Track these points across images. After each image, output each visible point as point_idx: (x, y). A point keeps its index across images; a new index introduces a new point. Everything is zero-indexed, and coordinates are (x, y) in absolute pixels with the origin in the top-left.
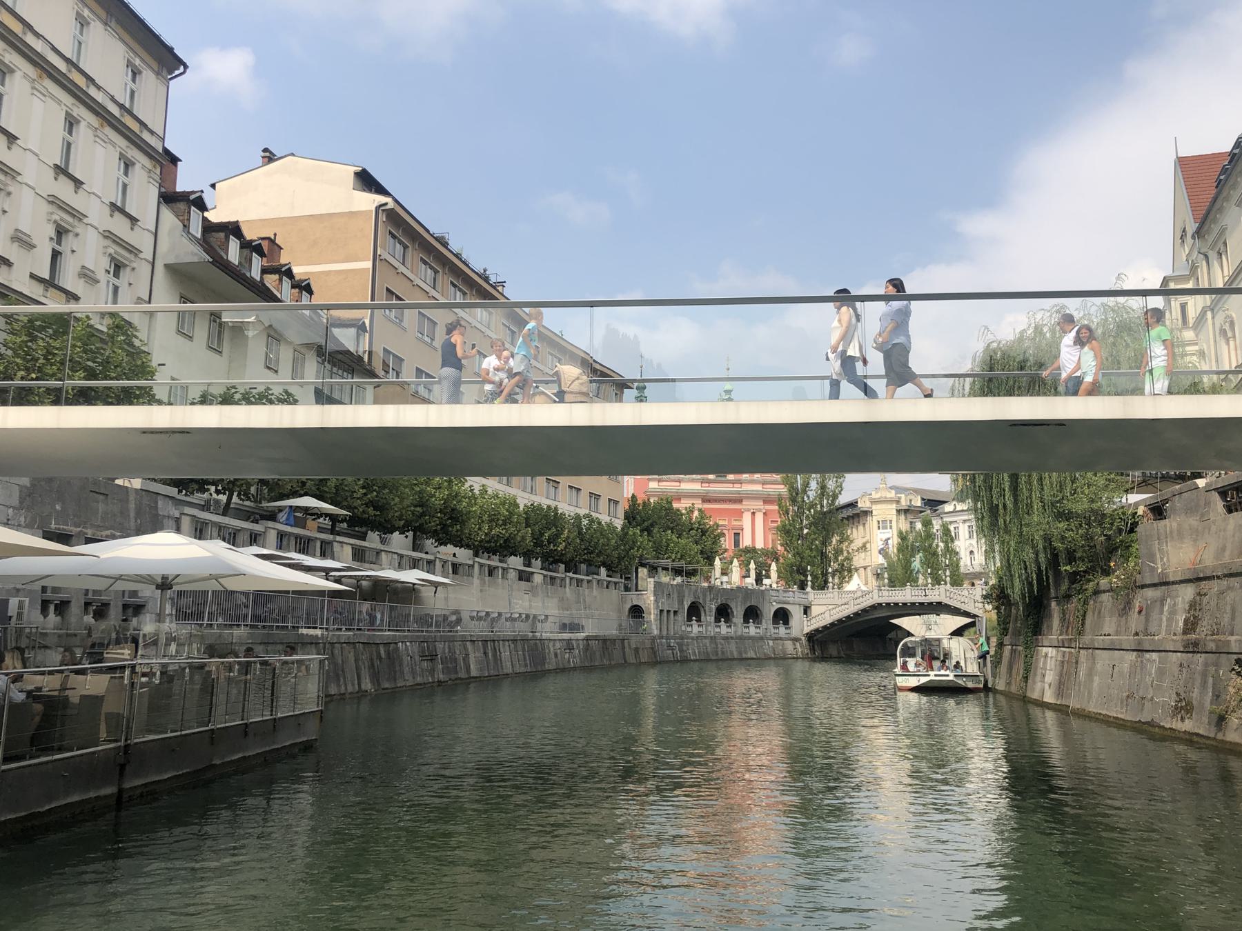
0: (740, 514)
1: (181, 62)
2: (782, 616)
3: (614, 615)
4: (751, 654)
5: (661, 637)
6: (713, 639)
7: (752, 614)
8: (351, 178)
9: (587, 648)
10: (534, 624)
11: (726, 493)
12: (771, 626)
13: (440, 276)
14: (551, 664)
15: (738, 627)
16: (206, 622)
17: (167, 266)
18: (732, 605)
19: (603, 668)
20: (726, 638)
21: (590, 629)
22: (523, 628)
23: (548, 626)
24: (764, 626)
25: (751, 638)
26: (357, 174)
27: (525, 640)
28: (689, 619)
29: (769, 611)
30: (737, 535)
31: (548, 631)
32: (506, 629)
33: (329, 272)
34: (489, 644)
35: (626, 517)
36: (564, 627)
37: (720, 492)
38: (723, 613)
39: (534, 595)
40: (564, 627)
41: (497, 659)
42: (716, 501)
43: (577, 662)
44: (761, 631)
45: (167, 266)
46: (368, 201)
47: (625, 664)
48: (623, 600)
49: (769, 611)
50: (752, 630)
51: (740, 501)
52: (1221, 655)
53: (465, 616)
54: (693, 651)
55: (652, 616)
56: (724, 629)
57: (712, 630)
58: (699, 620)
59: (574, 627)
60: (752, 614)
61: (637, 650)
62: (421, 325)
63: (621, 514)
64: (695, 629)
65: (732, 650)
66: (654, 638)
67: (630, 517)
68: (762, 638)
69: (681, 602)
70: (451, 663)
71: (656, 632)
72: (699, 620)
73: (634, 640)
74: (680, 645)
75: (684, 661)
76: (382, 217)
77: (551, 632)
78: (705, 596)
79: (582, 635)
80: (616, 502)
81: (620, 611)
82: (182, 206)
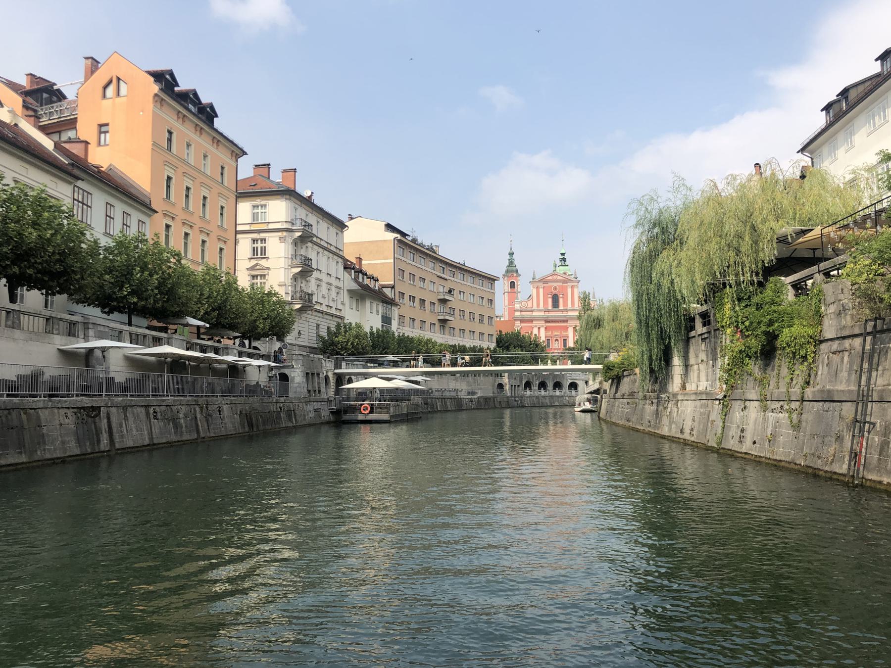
0: (566, 328)
1: (346, 226)
2: (573, 386)
3: (491, 388)
4: (557, 404)
5: (512, 397)
6: (537, 397)
7: (558, 385)
8: (384, 227)
9: (478, 401)
10: (457, 393)
11: (558, 317)
12: (567, 391)
13: (415, 256)
14: (464, 407)
15: (550, 391)
16: (104, 393)
17: (348, 290)
18: (547, 382)
19: (485, 409)
20: (544, 397)
21: (480, 394)
22: (453, 394)
23: (463, 392)
24: (564, 391)
25: (558, 397)
26: (386, 225)
27: (455, 398)
28: (525, 388)
29: (566, 383)
30: (565, 340)
31: (463, 395)
32: (447, 394)
33: (377, 264)
34: (443, 399)
35: (497, 342)
36: (469, 393)
37: (555, 316)
38: (543, 385)
39: (457, 381)
40: (469, 393)
41: (446, 405)
42: (553, 321)
43: (475, 406)
44: (562, 393)
45: (348, 290)
46: (392, 236)
47: (495, 407)
48: (495, 381)
49: (566, 383)
50: (558, 393)
51: (566, 321)
52: (843, 403)
53: (434, 390)
54: (527, 402)
55: (507, 388)
56: (543, 392)
57: (537, 393)
58: (530, 389)
59: (473, 393)
60: (558, 385)
61: (500, 402)
62: (410, 277)
63: (495, 340)
64: (528, 393)
65: (547, 401)
66: (508, 397)
67: (499, 342)
68: (562, 396)
69: (521, 381)
70: (432, 406)
71: (509, 395)
72: (530, 389)
73: (499, 398)
74: (521, 400)
75: (523, 406)
76: (396, 242)
77: (865, 457)
78: (533, 378)
79: (476, 396)
80: (492, 335)
81: (493, 386)
82: (349, 270)
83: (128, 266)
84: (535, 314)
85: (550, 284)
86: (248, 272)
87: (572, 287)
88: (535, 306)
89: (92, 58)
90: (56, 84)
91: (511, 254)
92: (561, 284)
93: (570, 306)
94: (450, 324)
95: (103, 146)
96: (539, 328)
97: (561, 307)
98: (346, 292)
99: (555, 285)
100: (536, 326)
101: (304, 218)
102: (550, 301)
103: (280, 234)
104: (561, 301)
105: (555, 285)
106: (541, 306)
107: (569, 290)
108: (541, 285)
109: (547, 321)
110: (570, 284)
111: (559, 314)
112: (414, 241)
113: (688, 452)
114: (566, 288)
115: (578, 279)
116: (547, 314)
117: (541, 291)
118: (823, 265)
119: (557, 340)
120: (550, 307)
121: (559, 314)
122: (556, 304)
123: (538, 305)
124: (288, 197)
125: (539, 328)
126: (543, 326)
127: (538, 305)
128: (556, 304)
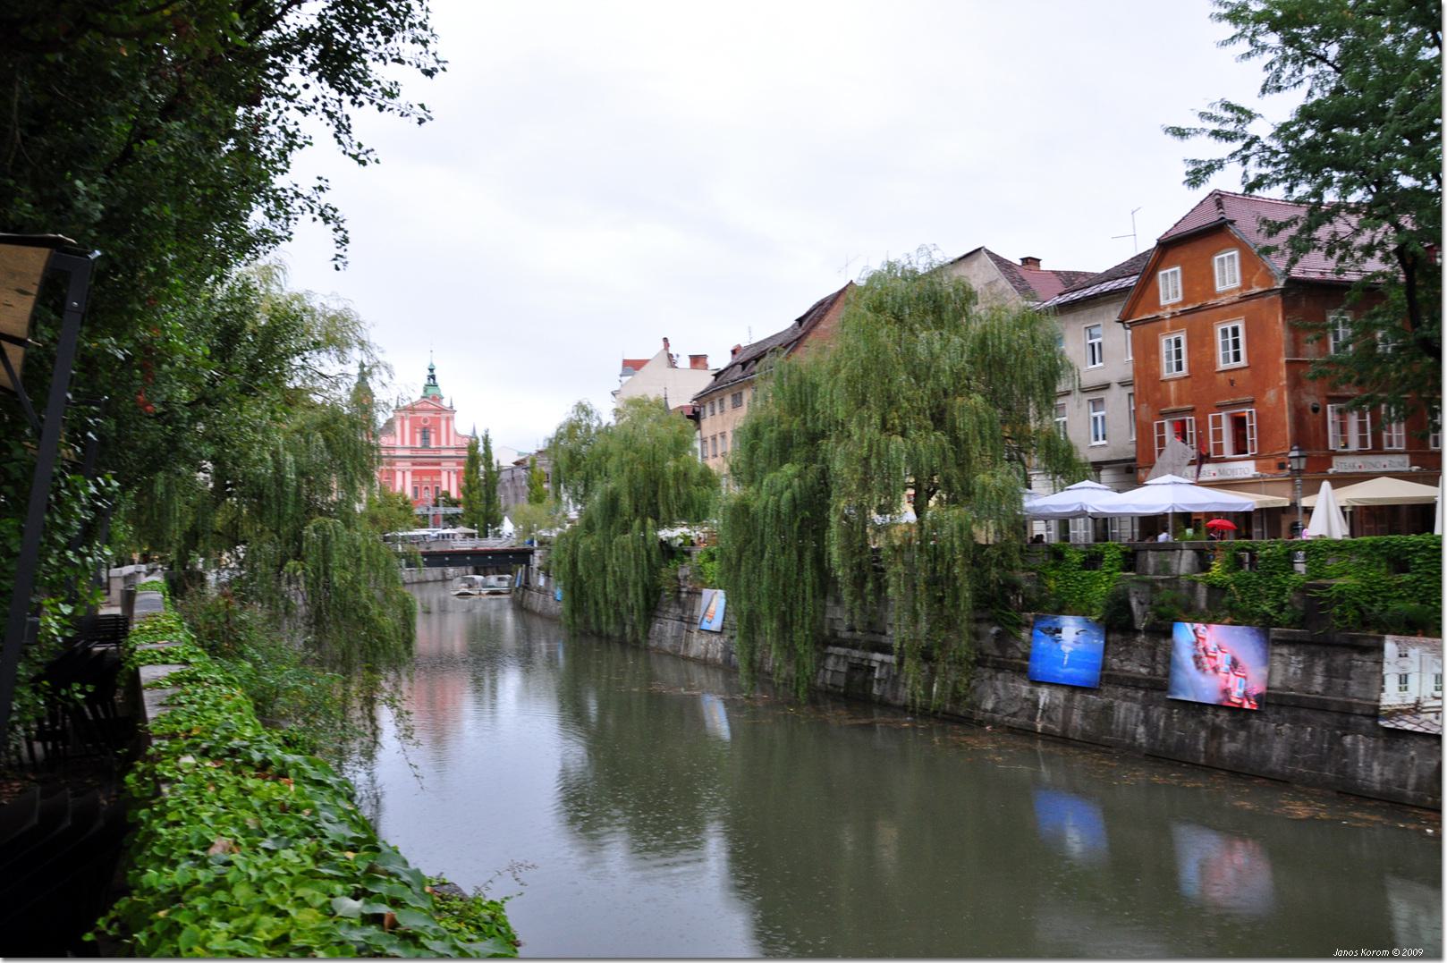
0: (439, 473)
84: (444, 453)
85: (418, 415)
86: (480, 434)
87: (448, 419)
88: (399, 444)
92: (432, 415)
93: (444, 444)
95: (1442, 730)
96: (404, 473)
97: (433, 446)
102: (418, 436)
104: (433, 437)
106: (407, 444)
107: (443, 423)
110: (444, 415)
113: (539, 609)
114: (438, 420)
116: (414, 454)
117: (407, 423)
118: (303, 869)
119: (427, 488)
122: (426, 438)
123: (448, 443)
125: (404, 473)
127: (448, 443)
128: (426, 438)
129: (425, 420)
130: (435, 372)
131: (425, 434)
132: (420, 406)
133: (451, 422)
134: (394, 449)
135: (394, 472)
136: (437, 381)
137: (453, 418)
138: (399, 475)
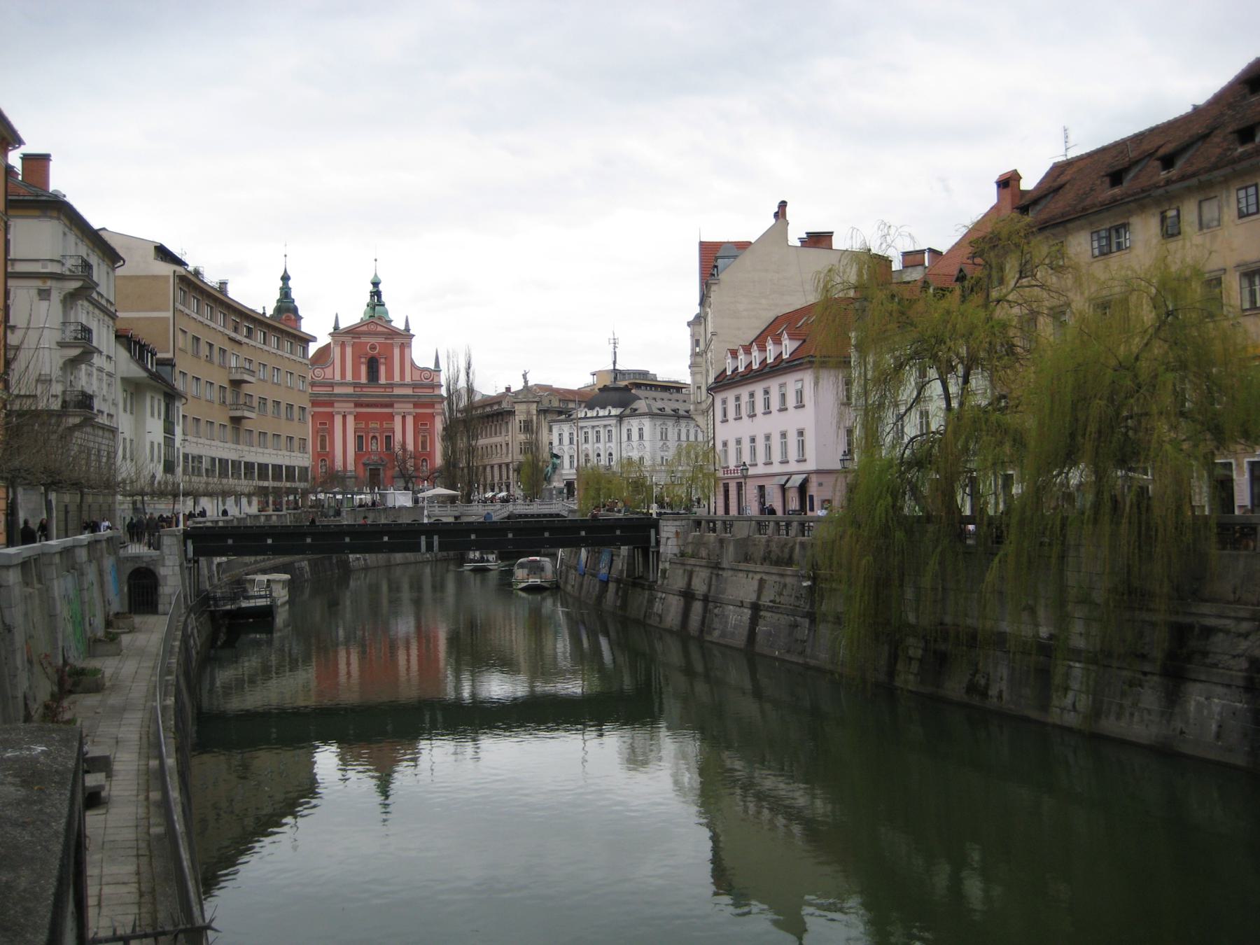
0: (391, 417)
17: (123, 379)
30: (388, 438)
45: (123, 379)
83: (7, 429)
84: (337, 390)
85: (364, 340)
88: (338, 377)
89: (777, 321)
90: (725, 370)
91: (285, 278)
92: (382, 340)
93: (397, 379)
94: (247, 425)
97: (383, 381)
98: (119, 382)
99: (373, 340)
100: (338, 413)
101: (85, 256)
102: (364, 369)
103: (38, 283)
104: (382, 369)
105: (373, 340)
106: (349, 377)
107: (397, 352)
108: (347, 339)
109: (357, 405)
111: (379, 391)
112: (197, 273)
115: (411, 332)
117: (349, 350)
119: (374, 437)
120: (364, 380)
121: (379, 391)
124: (55, 214)
125: (404, 417)
126: (350, 413)
129: (373, 348)
130: (381, 287)
131: (373, 365)
132: (365, 328)
133: (407, 350)
134: (332, 385)
135: (331, 416)
136: (384, 298)
137: (410, 346)
138: (338, 421)
